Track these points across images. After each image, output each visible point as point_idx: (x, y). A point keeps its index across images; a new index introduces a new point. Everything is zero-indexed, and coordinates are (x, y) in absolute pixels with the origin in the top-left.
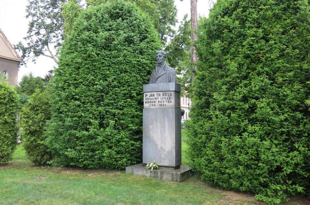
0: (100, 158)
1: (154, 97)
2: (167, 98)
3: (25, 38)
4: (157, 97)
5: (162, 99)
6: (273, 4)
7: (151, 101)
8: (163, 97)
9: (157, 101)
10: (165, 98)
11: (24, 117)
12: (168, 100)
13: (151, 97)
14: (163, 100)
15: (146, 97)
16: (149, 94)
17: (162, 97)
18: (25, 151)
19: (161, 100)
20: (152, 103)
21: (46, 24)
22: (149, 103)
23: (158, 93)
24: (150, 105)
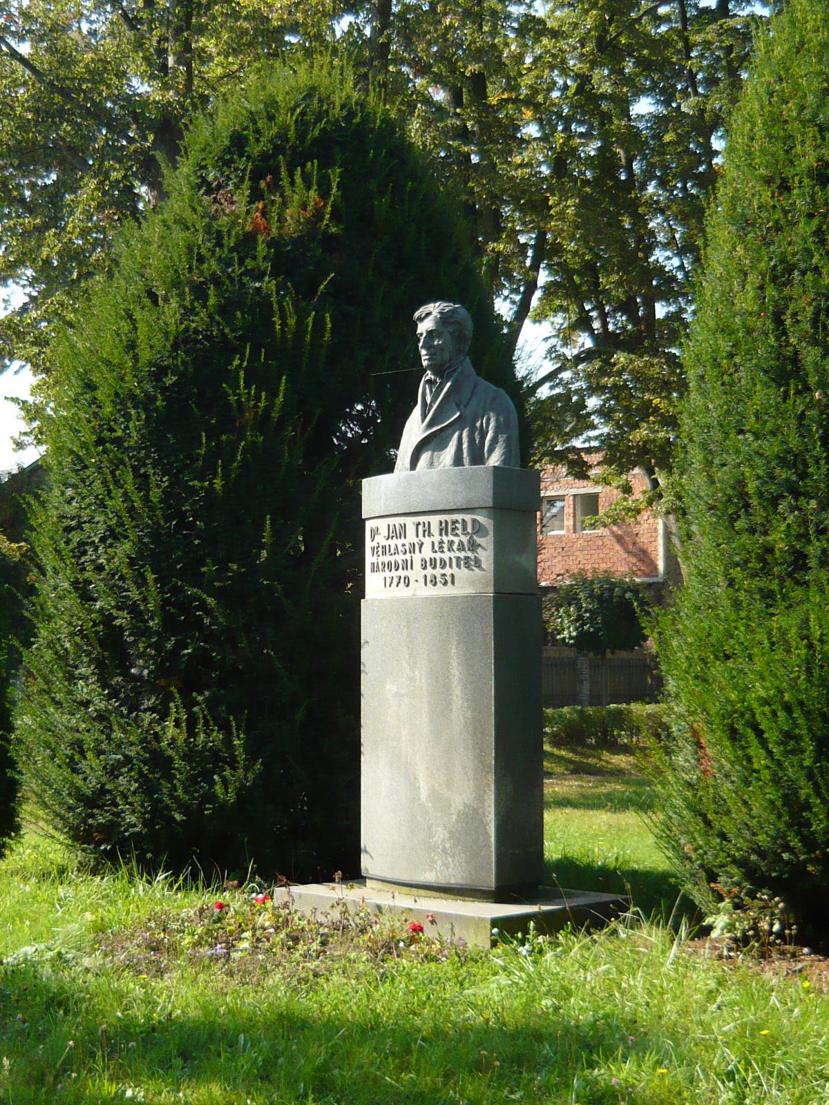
0: (52, 642)
1: (403, 540)
2: (461, 543)
3: (6, 398)
4: (416, 540)
5: (436, 548)
6: (535, 139)
7: (392, 559)
8: (441, 542)
9: (417, 557)
10: (451, 543)
11: (772, 630)
12: (462, 555)
13: (393, 542)
14: (443, 555)
15: (375, 544)
16: (382, 525)
17: (437, 538)
18: (586, 1018)
19: (433, 555)
20: (443, 567)
21: (17, 364)
22: (383, 570)
23: (422, 519)
24: (388, 580)
